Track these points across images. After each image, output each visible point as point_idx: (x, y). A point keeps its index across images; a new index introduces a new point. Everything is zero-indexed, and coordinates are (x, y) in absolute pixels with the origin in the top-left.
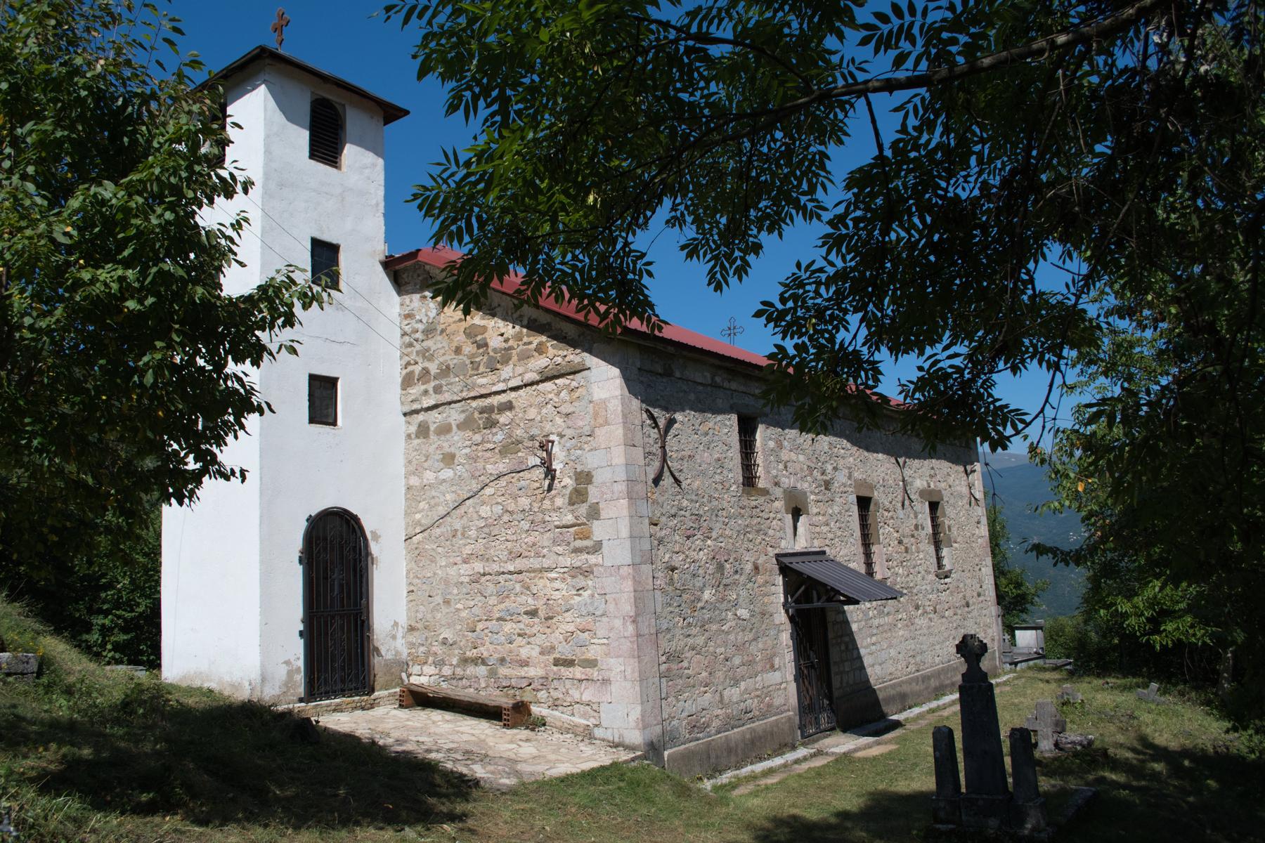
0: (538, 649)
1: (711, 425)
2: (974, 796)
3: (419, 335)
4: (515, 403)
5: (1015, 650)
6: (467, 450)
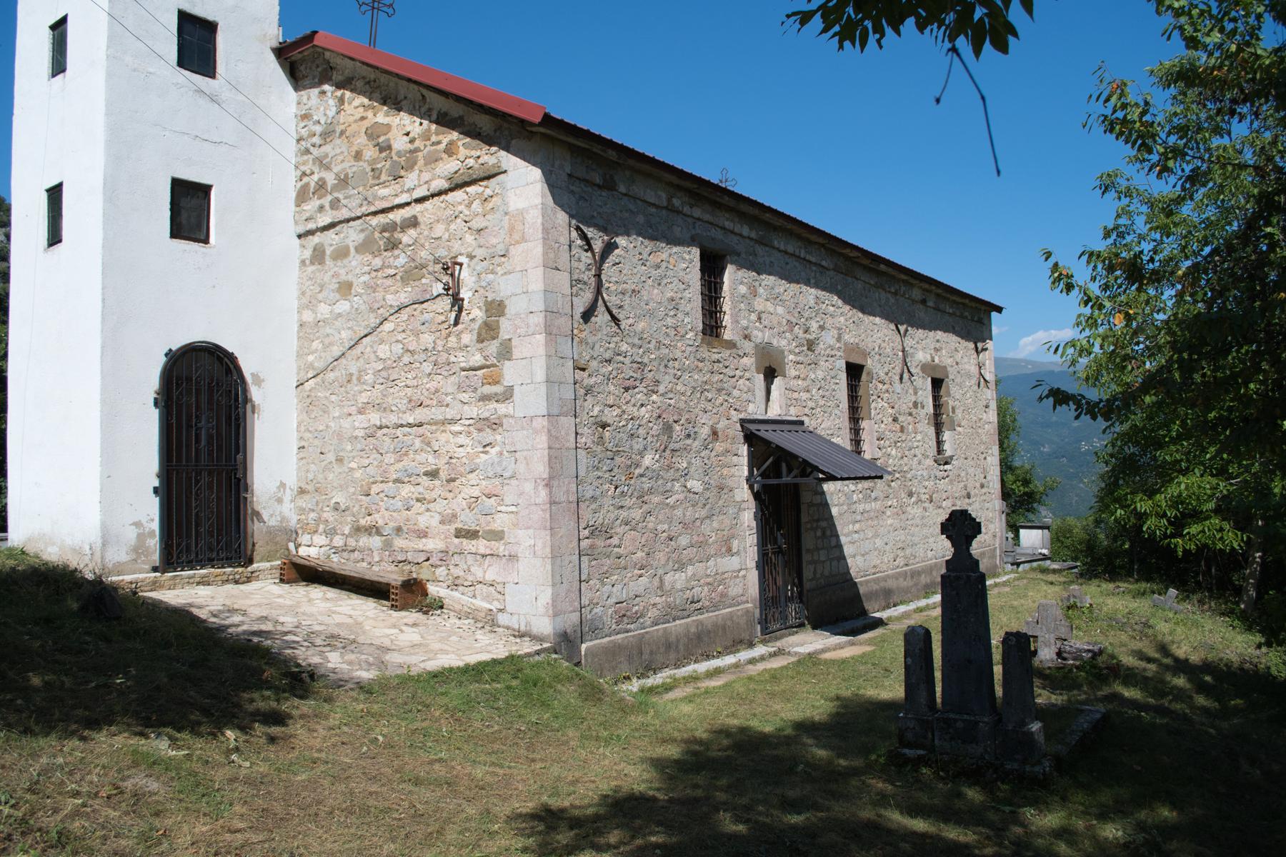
0: (438, 518)
1: (664, 256)
2: (952, 716)
3: (316, 140)
4: (420, 219)
5: (1018, 550)
6: (366, 278)
